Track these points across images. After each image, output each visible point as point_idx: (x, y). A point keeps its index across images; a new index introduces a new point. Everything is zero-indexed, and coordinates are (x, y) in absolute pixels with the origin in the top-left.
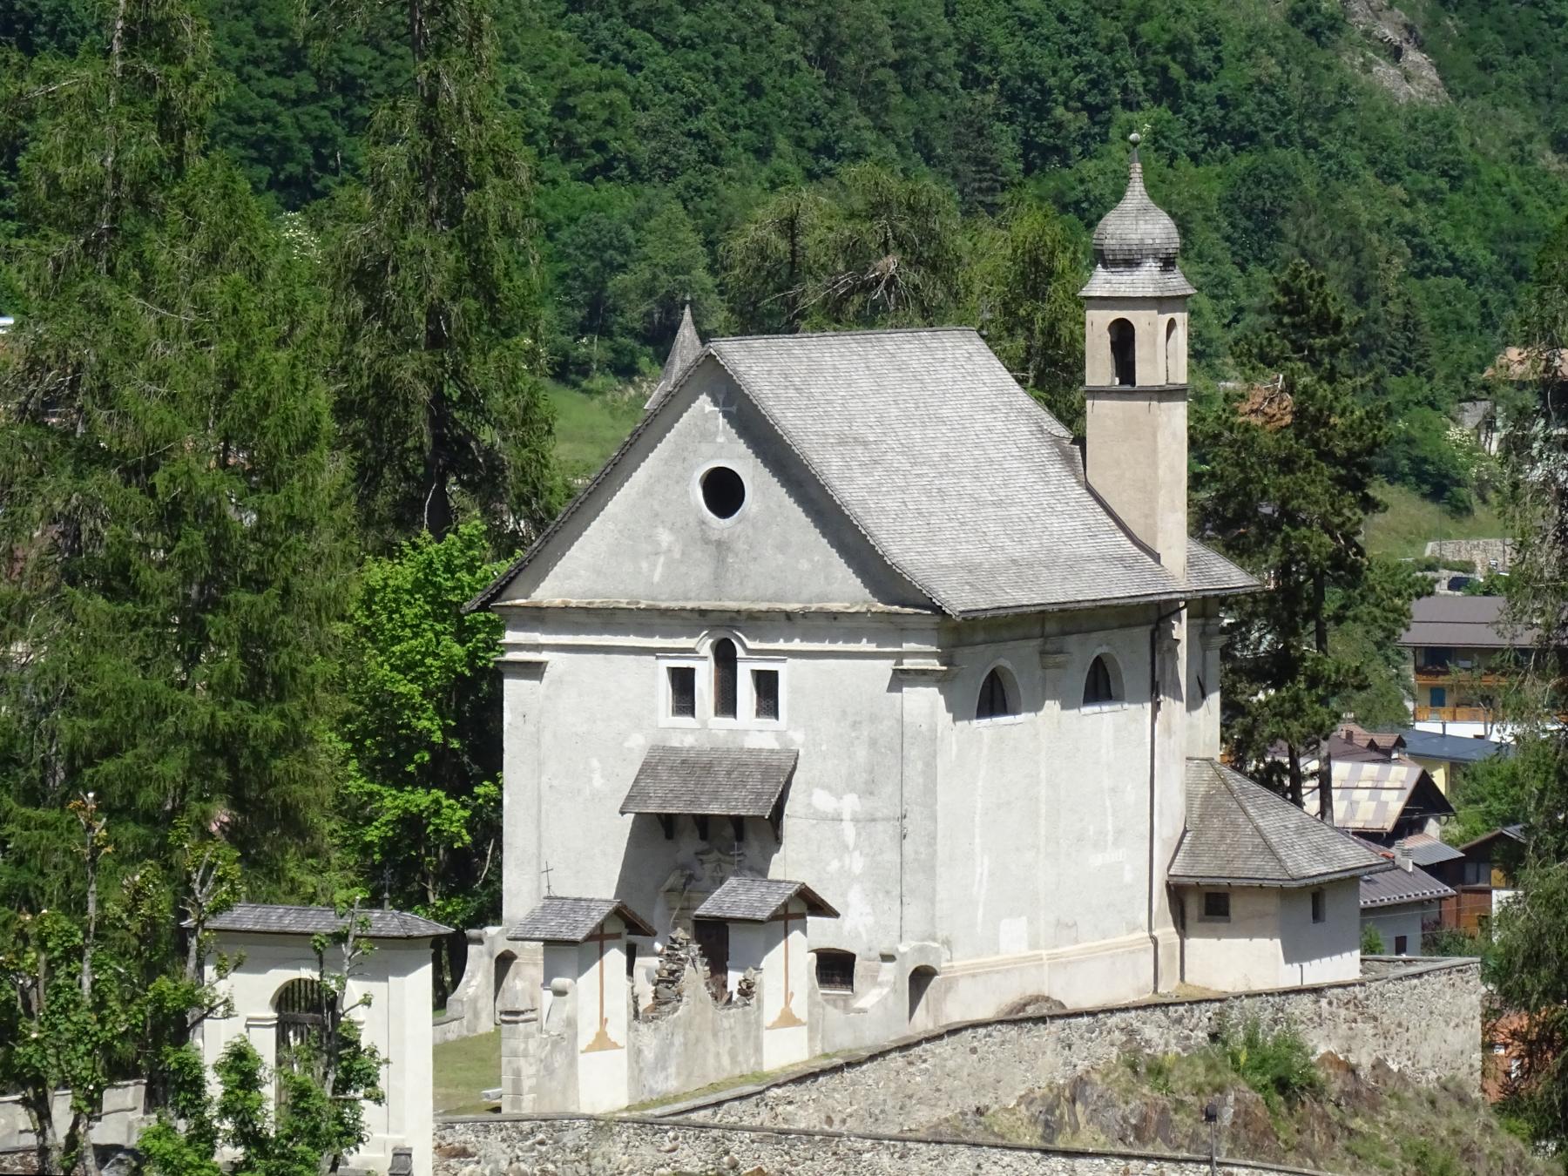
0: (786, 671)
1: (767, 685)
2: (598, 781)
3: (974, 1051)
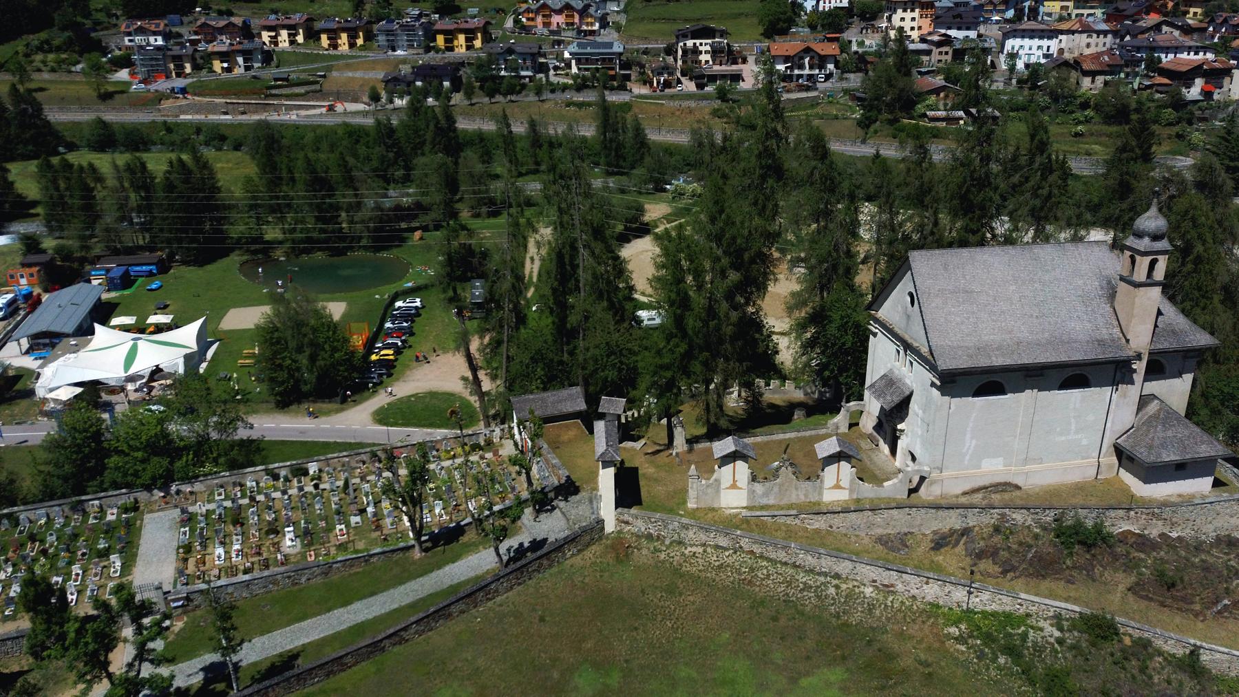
1: (911, 363)
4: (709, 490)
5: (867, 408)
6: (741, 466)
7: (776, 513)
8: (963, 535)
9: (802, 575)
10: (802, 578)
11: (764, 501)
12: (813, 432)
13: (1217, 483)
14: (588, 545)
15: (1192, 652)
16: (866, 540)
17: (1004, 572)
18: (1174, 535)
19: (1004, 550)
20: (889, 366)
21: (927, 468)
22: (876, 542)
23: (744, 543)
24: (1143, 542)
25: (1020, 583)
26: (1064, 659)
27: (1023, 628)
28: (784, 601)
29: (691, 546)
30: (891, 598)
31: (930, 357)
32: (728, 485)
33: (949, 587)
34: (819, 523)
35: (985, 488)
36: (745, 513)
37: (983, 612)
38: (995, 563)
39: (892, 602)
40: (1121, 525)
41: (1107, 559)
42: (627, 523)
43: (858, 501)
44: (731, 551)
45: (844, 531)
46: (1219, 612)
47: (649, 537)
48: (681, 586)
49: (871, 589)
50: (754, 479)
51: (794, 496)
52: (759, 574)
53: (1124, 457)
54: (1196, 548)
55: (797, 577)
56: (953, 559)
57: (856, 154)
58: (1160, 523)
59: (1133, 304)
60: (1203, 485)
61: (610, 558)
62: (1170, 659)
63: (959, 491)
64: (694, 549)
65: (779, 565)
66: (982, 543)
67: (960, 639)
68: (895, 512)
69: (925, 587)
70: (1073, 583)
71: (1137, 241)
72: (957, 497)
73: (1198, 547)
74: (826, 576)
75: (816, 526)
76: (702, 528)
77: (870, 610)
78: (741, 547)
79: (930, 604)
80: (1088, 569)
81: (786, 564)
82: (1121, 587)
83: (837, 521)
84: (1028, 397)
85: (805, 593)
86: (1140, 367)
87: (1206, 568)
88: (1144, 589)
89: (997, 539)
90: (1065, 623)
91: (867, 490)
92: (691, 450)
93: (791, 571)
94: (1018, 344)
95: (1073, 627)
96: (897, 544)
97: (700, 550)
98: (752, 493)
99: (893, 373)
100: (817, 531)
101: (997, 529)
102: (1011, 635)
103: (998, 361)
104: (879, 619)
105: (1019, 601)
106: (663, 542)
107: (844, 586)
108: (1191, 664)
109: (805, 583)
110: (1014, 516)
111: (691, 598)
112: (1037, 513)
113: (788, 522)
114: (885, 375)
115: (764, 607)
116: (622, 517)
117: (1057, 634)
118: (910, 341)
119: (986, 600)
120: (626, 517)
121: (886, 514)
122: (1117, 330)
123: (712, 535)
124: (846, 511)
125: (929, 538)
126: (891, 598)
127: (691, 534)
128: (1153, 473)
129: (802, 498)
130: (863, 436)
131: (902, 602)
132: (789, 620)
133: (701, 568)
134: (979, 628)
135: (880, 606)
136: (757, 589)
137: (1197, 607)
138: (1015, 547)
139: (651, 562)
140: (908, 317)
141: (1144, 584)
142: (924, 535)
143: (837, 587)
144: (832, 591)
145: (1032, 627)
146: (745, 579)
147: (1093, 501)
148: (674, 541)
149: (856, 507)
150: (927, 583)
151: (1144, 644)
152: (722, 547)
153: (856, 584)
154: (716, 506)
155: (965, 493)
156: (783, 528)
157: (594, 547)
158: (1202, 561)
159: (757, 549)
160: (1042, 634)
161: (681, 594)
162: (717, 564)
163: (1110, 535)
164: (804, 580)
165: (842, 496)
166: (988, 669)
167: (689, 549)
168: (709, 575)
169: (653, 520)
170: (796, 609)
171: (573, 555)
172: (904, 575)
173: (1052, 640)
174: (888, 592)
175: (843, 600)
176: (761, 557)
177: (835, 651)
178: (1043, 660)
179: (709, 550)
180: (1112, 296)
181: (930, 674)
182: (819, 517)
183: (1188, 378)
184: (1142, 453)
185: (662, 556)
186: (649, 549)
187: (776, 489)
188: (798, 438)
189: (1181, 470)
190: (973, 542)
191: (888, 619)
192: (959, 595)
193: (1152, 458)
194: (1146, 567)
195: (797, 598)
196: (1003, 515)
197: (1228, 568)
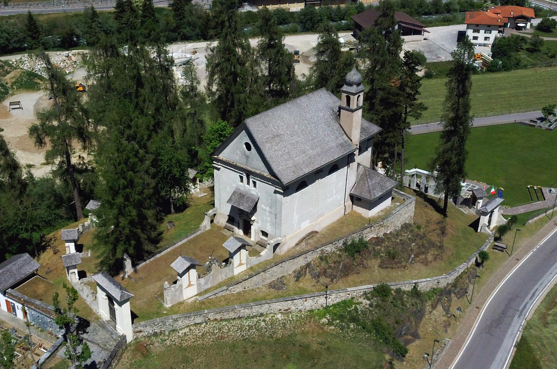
0: (257, 182)
1: (254, 183)
2: (229, 190)
3: (282, 267)
4: (177, 293)
5: (219, 212)
6: (193, 273)
7: (216, 291)
8: (306, 268)
9: (245, 321)
10: (246, 323)
11: (206, 287)
12: (194, 235)
13: (393, 198)
14: (122, 354)
15: (414, 287)
16: (264, 289)
17: (332, 281)
18: (388, 232)
19: (328, 269)
20: (234, 185)
21: (279, 238)
22: (269, 288)
23: (211, 316)
24: (378, 241)
25: (340, 284)
26: (376, 314)
27: (354, 306)
28: (243, 340)
29: (181, 329)
30: (290, 316)
31: (272, 178)
32: (187, 285)
33: (316, 298)
34: (238, 289)
35: (304, 238)
36: (200, 298)
37: (333, 305)
38: (326, 277)
39: (292, 318)
40: (369, 235)
41: (367, 254)
42: (140, 331)
43: (251, 268)
44: (205, 324)
45: (251, 288)
46: (411, 262)
47: (155, 334)
48: (190, 356)
49: (280, 315)
50: (199, 277)
51: (220, 278)
52: (224, 330)
53: (355, 199)
54: (397, 235)
55: (243, 324)
56: (307, 282)
57: (12, 14)
58: (383, 228)
59: (352, 121)
60: (388, 203)
61: (139, 357)
62: (408, 293)
63: (294, 245)
64: (184, 331)
65: (232, 321)
66: (319, 269)
67: (330, 324)
68: (275, 268)
69: (305, 303)
70: (359, 273)
71: (350, 88)
72: (294, 248)
73: (397, 234)
74: (256, 317)
75: (238, 290)
76: (186, 317)
77: (284, 326)
78: (209, 319)
79: (309, 311)
80: (361, 264)
81: (234, 319)
82: (376, 267)
83: (248, 284)
84: (319, 183)
85: (251, 331)
86: (356, 152)
87: (403, 243)
88: (384, 264)
89: (323, 264)
90: (368, 295)
91: (255, 260)
92: (136, 271)
93: (238, 322)
94: (310, 158)
95: (373, 296)
96: (280, 285)
97: (187, 330)
98: (199, 285)
99: (239, 189)
100: (239, 294)
101: (321, 258)
102: (350, 311)
103: (307, 170)
104: (290, 330)
105: (348, 293)
106: (164, 335)
107: (267, 319)
108: (415, 293)
109: (248, 326)
110: (327, 249)
111: (199, 360)
112: (335, 244)
113: (223, 294)
114: (234, 193)
115: (237, 348)
116: (137, 330)
117: (368, 302)
118: (253, 170)
119: (334, 299)
120: (140, 328)
121: (271, 271)
122: (345, 136)
123: (192, 319)
124: (251, 276)
125: (293, 275)
126: (290, 316)
127: (180, 323)
128: (370, 205)
129: (224, 277)
130: (219, 228)
131: (296, 316)
132: (253, 349)
133: (193, 340)
134: (336, 314)
135: (288, 322)
136: (227, 339)
137: (404, 264)
138: (333, 265)
139: (163, 349)
140: (247, 157)
141: (384, 262)
142: (290, 275)
143: (264, 321)
144: (263, 324)
145: (357, 304)
146: (219, 336)
147: (352, 228)
148: (171, 331)
149: (253, 272)
150: (306, 301)
151: (398, 291)
152: (199, 324)
153: (272, 315)
154: (181, 300)
155: (297, 245)
156: (222, 298)
157: (125, 355)
158: (401, 240)
159: (218, 317)
160: (363, 305)
161: (193, 361)
162: (200, 334)
163: (367, 242)
164: (247, 324)
165: (243, 268)
166: (348, 333)
167: (181, 332)
168: (199, 342)
169: (156, 324)
170: (251, 342)
171: (116, 365)
172: (294, 301)
173: (367, 306)
174: (288, 313)
175: (270, 327)
176: (221, 320)
177: (282, 356)
178: (368, 318)
179: (192, 328)
180: (338, 116)
181: (328, 348)
182: (239, 285)
183: (370, 149)
184: (365, 195)
185: (168, 342)
186: (158, 342)
187: (211, 278)
188: (188, 241)
189: (382, 199)
190: (313, 270)
191: (294, 327)
192: (322, 301)
193: (373, 197)
194: (382, 253)
195: (249, 336)
196: (322, 251)
197: (409, 239)
